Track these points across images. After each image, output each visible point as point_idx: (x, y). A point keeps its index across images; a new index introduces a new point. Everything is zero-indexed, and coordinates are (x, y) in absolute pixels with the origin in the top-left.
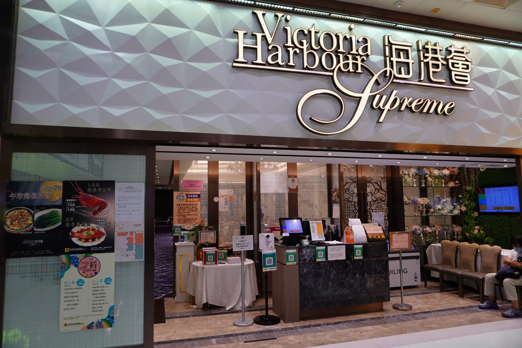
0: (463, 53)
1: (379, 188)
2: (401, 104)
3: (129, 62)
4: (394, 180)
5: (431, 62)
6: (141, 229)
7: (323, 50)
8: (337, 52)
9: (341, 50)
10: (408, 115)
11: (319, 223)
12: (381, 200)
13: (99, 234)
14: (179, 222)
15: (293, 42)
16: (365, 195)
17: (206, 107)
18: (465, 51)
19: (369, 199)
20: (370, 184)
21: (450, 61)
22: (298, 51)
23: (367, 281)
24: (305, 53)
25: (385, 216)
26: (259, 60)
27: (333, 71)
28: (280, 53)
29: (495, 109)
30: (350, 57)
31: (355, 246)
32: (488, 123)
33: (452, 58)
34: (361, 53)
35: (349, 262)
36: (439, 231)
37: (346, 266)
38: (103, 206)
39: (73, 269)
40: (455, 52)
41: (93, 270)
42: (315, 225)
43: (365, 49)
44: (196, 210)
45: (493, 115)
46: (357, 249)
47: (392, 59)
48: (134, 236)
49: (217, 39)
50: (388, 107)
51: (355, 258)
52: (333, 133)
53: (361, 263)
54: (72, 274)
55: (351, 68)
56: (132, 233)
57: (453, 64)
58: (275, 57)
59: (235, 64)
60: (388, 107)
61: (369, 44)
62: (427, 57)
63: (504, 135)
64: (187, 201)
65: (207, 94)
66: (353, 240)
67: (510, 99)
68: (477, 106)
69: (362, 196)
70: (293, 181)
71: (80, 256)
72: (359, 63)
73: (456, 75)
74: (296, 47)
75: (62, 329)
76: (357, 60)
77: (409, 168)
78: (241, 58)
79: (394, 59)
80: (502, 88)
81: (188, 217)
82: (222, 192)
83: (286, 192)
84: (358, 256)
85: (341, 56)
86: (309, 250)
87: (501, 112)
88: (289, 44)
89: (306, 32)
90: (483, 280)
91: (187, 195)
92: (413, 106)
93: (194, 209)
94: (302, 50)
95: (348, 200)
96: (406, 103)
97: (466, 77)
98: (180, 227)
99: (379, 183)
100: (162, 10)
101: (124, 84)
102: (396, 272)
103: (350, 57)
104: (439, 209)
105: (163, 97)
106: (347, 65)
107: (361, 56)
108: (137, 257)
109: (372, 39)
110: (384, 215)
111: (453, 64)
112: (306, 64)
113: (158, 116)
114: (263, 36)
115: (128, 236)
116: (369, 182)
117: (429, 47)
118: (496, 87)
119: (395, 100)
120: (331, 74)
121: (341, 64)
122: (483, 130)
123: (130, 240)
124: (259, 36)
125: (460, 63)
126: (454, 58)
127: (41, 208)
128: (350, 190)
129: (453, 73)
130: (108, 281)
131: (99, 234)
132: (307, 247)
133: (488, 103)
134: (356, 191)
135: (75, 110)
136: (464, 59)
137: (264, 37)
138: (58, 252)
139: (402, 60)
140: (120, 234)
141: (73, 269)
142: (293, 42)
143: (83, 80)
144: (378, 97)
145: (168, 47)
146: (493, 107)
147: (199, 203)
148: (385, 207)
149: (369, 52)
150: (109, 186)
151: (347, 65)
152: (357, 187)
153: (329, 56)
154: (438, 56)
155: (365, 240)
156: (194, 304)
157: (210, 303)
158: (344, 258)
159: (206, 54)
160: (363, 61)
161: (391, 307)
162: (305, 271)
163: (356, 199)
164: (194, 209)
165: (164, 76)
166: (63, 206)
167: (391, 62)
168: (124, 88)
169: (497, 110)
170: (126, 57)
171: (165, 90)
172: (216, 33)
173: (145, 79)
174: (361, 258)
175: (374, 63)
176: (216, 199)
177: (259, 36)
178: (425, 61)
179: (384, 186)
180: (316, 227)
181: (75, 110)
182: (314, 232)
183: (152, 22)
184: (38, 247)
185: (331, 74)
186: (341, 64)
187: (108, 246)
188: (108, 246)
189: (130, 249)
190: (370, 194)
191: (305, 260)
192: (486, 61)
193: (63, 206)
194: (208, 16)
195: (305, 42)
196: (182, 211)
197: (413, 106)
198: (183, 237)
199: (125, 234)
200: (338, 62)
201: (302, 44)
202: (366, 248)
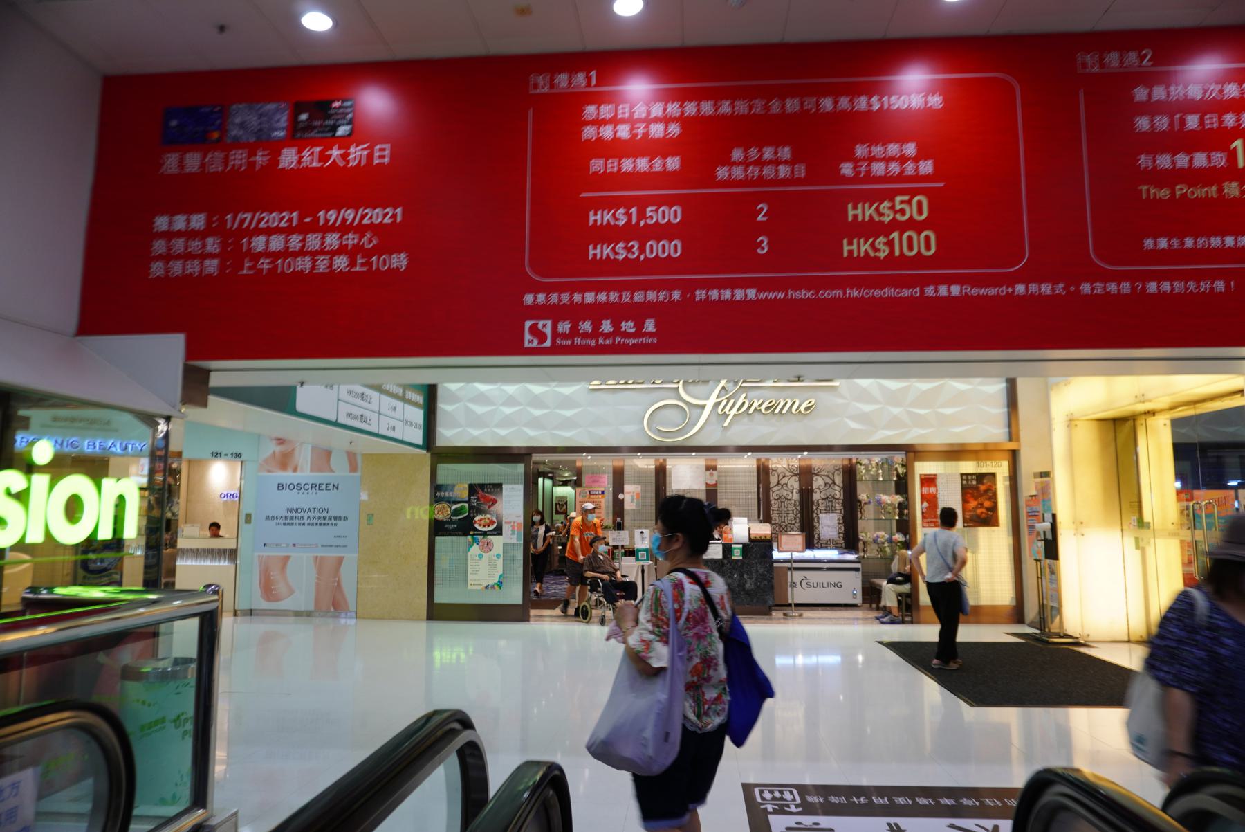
2: (749, 407)
4: (850, 474)
6: (521, 520)
13: (492, 522)
17: (568, 423)
19: (816, 496)
32: (862, 418)
37: (723, 565)
38: (495, 502)
39: (475, 546)
41: (489, 547)
50: (734, 411)
54: (475, 549)
60: (734, 411)
69: (806, 493)
70: (711, 475)
71: (480, 537)
75: (469, 587)
77: (779, 463)
82: (627, 488)
83: (704, 487)
84: (737, 555)
90: (312, 471)
92: (763, 408)
101: (508, 410)
113: (531, 433)
123: (513, 527)
127: (455, 502)
130: (498, 556)
131: (492, 522)
134: (796, 485)
135: (475, 432)
138: (466, 534)
141: (475, 546)
143: (480, 410)
148: (838, 506)
150: (498, 486)
155: (746, 540)
158: (720, 556)
163: (796, 496)
166: (469, 502)
169: (876, 401)
171: (537, 412)
176: (621, 496)
179: (839, 479)
181: (475, 432)
184: (454, 530)
187: (498, 531)
188: (498, 531)
189: (513, 533)
193: (469, 502)
197: (763, 408)
202: (746, 548)
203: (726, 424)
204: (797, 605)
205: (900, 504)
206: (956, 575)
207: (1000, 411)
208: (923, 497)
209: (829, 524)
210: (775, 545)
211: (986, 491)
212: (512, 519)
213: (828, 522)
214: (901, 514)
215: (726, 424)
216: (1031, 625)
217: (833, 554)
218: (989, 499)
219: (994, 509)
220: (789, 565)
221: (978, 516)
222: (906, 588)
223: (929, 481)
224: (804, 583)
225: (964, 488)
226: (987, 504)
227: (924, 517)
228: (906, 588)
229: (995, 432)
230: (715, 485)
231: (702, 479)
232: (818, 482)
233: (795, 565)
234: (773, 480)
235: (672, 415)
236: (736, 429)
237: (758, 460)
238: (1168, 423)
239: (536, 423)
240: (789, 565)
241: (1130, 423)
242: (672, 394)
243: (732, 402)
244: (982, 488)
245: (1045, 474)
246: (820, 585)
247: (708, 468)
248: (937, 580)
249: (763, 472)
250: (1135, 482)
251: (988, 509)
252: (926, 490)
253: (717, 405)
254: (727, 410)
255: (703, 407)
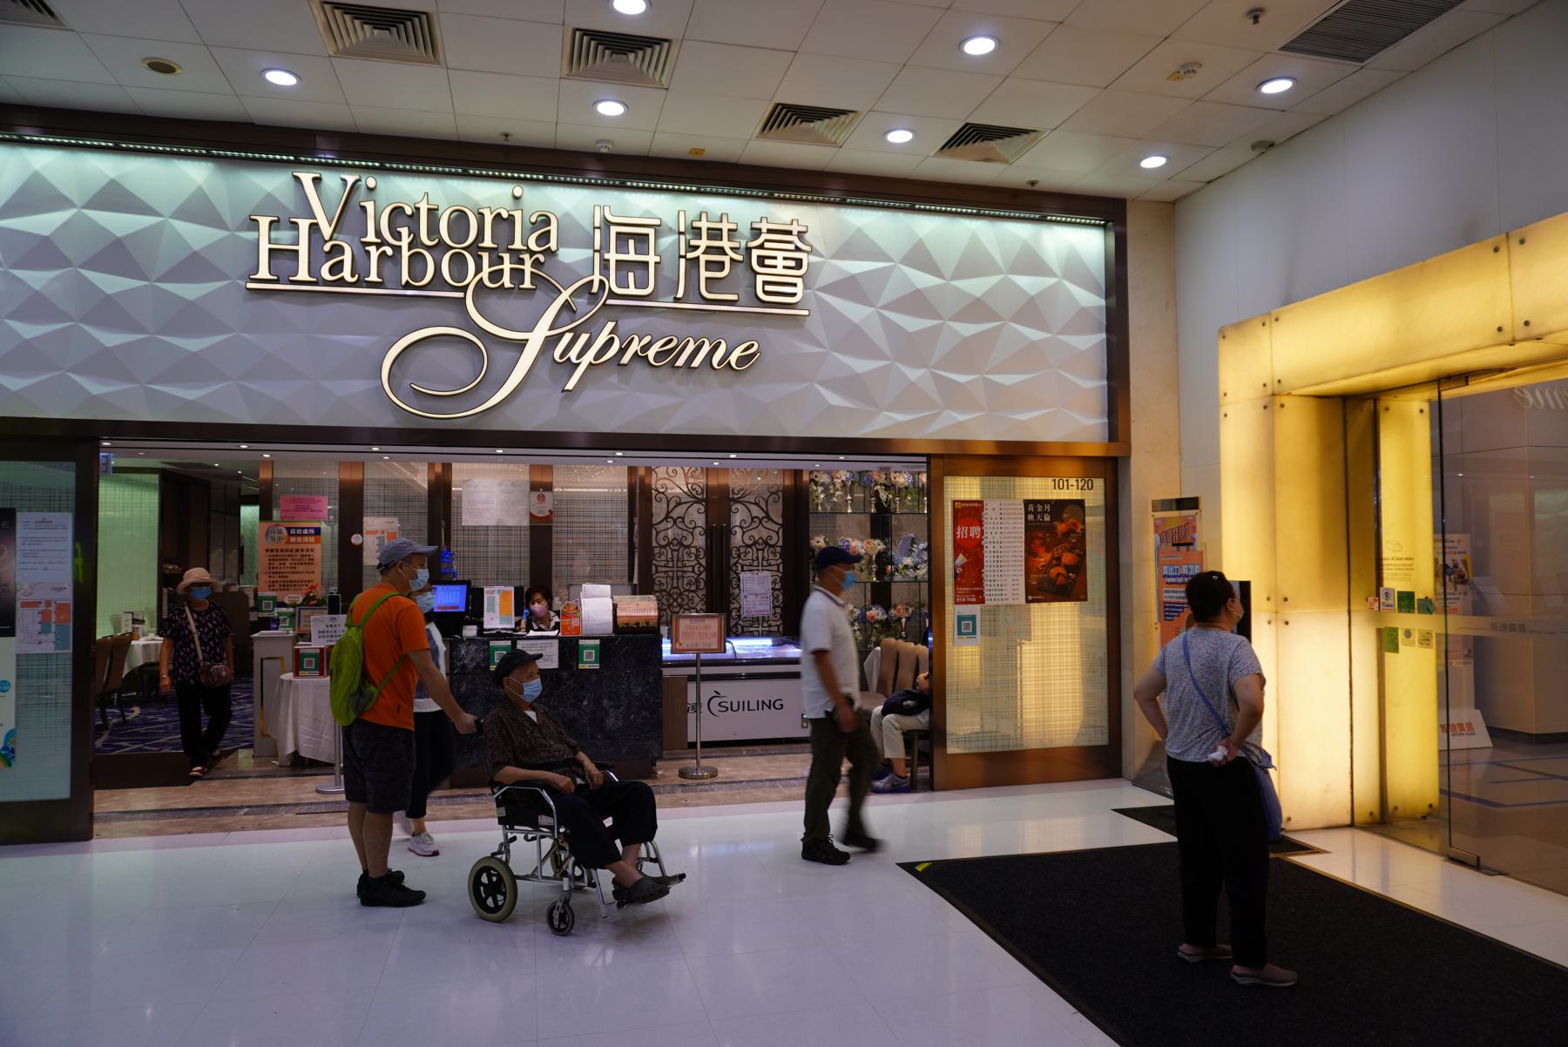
0: (789, 233)
1: (761, 514)
2: (622, 351)
3: (37, 287)
4: (796, 504)
5: (703, 259)
7: (441, 247)
8: (476, 248)
9: (488, 243)
10: (640, 371)
11: (507, 593)
12: (766, 543)
14: (271, 587)
15: (378, 234)
16: (727, 532)
17: (192, 369)
18: (795, 229)
19: (737, 539)
20: (739, 506)
21: (755, 253)
22: (389, 251)
23: (607, 714)
24: (406, 254)
25: (774, 582)
26: (303, 275)
27: (464, 289)
28: (347, 258)
29: (870, 351)
30: (506, 257)
31: (582, 642)
32: (850, 385)
33: (761, 247)
34: (534, 247)
35: (565, 674)
36: (908, 619)
40: (770, 231)
42: (497, 597)
43: (545, 237)
44: (311, 561)
45: (861, 366)
46: (586, 647)
47: (607, 256)
48: (53, 608)
49: (215, 234)
50: (589, 357)
51: (581, 666)
52: (461, 415)
53: (594, 678)
55: (506, 280)
56: (48, 603)
57: (761, 260)
58: (337, 268)
59: (250, 285)
60: (589, 357)
61: (553, 228)
62: (696, 248)
63: (890, 409)
64: (288, 542)
65: (193, 345)
66: (578, 629)
67: (910, 330)
68: (819, 344)
69: (718, 534)
70: (541, 498)
72: (528, 268)
73: (765, 283)
74: (384, 243)
76: (522, 262)
77: (675, 478)
78: (264, 273)
79: (613, 256)
80: (895, 306)
81: (292, 577)
82: (371, 522)
83: (526, 523)
85: (485, 256)
86: (473, 648)
87: (885, 358)
88: (371, 237)
89: (409, 211)
91: (288, 529)
92: (651, 353)
93: (306, 560)
94: (397, 249)
95: (681, 544)
96: (635, 347)
97: (795, 285)
98: (273, 599)
99: (763, 504)
100: (103, 182)
102: (754, 706)
103: (506, 257)
104: (906, 567)
105: (107, 353)
106: (496, 276)
107: (532, 253)
108: (58, 643)
109: (567, 215)
110: (770, 579)
111: (761, 260)
112: (405, 277)
113: (95, 388)
114: (311, 225)
115: (42, 608)
116: (737, 501)
117: (704, 225)
118: (881, 303)
119: (610, 342)
120: (461, 295)
121: (486, 270)
122: (834, 399)
123: (45, 616)
124: (304, 224)
125: (780, 255)
126: (767, 245)
128: (687, 521)
129: (760, 279)
132: (471, 640)
133: (854, 339)
134: (700, 520)
136: (792, 247)
137: (314, 228)
139: (632, 256)
140: (25, 605)
142: (378, 234)
144: (568, 337)
145: (116, 255)
146: (865, 348)
147: (317, 547)
149: (553, 245)
151: (496, 276)
152: (706, 511)
153: (458, 260)
154: (725, 243)
155: (609, 630)
156: (275, 756)
157: (303, 754)
159: (194, 266)
160: (536, 263)
161: (677, 772)
162: (463, 689)
163: (700, 541)
164: (306, 560)
165: (109, 312)
167: (605, 264)
168: (27, 336)
170: (37, 279)
171: (111, 339)
172: (218, 223)
173: (70, 319)
174: (597, 666)
175: (567, 267)
176: (356, 539)
177: (304, 224)
178: (690, 255)
179: (776, 512)
180: (497, 600)
182: (492, 610)
183: (86, 207)
185: (461, 295)
186: (485, 274)
189: (45, 629)
190: (738, 530)
191: (464, 666)
192: (854, 247)
194: (200, 189)
195: (404, 231)
196: (277, 564)
197: (651, 353)
198: (277, 621)
199: (35, 604)
200: (479, 269)
201: (398, 236)
202: (607, 645)
203: (570, 386)
204: (705, 745)
205: (879, 555)
206: (1241, 743)
207: (1094, 385)
208: (959, 547)
209: (756, 590)
210: (664, 630)
211: (1067, 534)
212: (41, 595)
213: (756, 588)
214: (881, 573)
215: (570, 386)
216: (1138, 782)
217: (758, 646)
218: (1071, 550)
219: (1079, 567)
220: (692, 671)
221: (1052, 582)
222: (921, 720)
223: (970, 513)
224: (715, 702)
225: (1029, 528)
226: (1068, 558)
227: (957, 584)
228: (921, 720)
229: (1075, 420)
230: (548, 518)
231: (523, 507)
232: (738, 516)
233: (705, 670)
234: (659, 510)
235: (453, 361)
236: (590, 396)
237: (632, 471)
238: (1426, 407)
239: (104, 363)
240: (692, 671)
241: (1369, 405)
242: (451, 315)
243: (584, 338)
244: (1061, 528)
245: (1192, 503)
246: (745, 706)
247: (534, 487)
248: (1191, 757)
249: (640, 496)
250: (1373, 512)
251: (1068, 568)
252: (962, 532)
253: (551, 342)
254: (573, 355)
255: (522, 344)
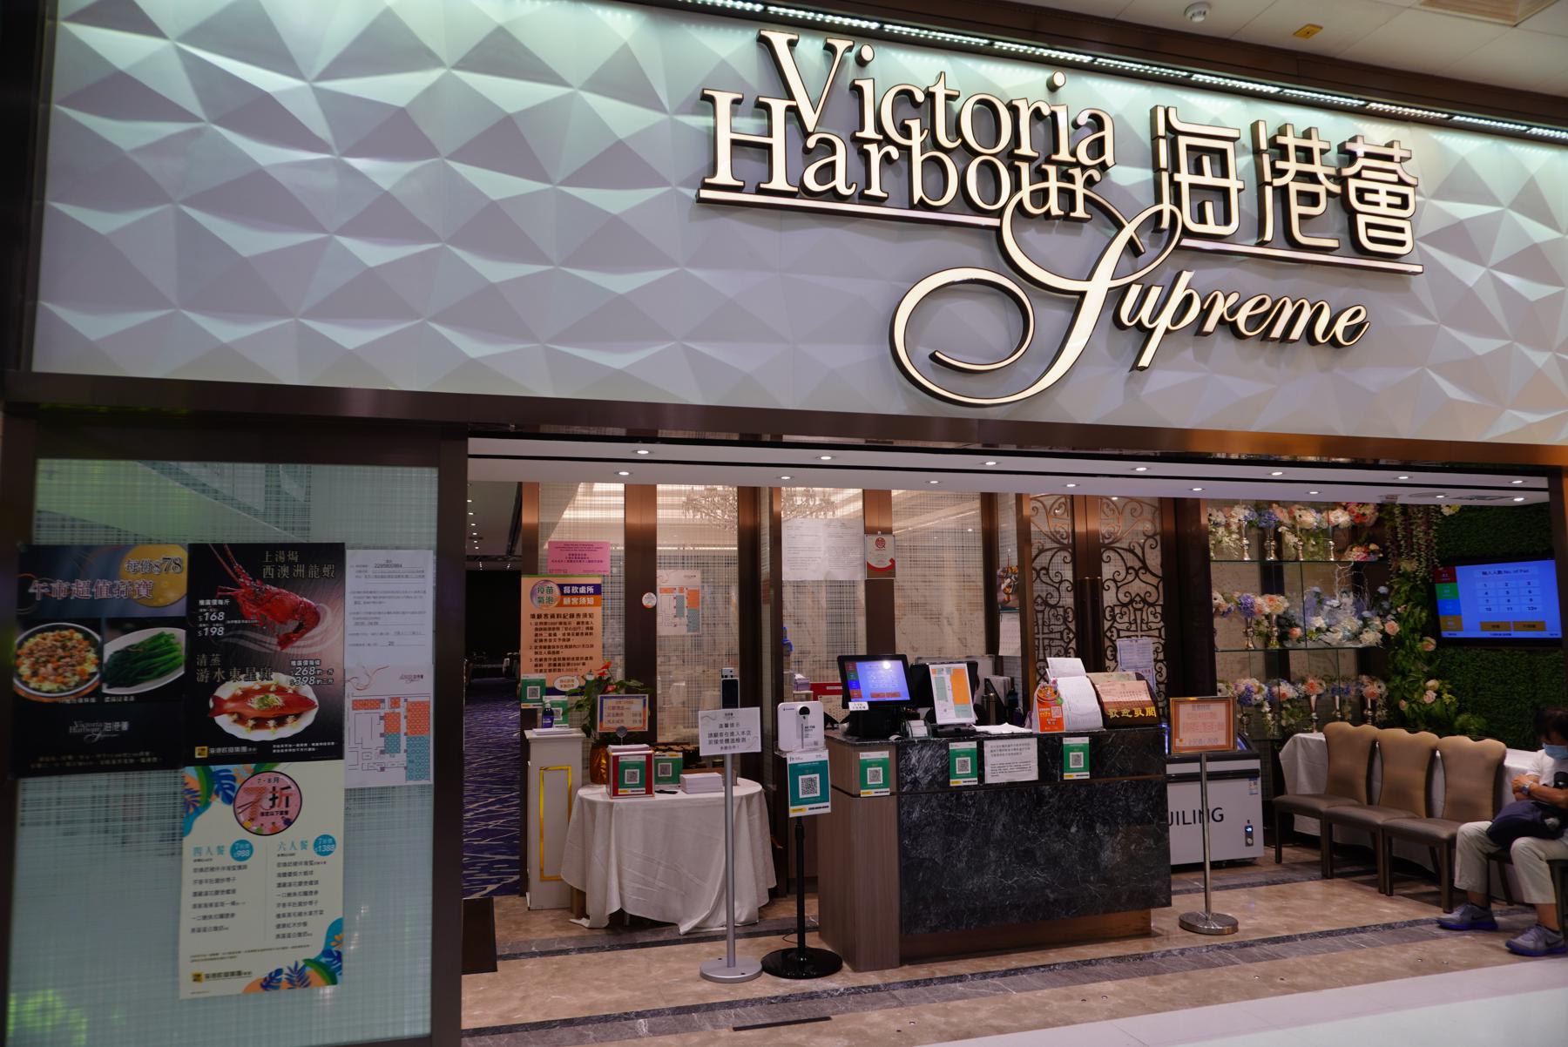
0: (1390, 158)
1: (1137, 564)
2: (1205, 314)
3: (386, 185)
4: (1182, 540)
5: (1294, 187)
6: (425, 690)
7: (969, 152)
8: (1011, 157)
9: (1025, 150)
10: (1224, 345)
11: (957, 671)
12: (1144, 601)
13: (297, 705)
14: (538, 667)
15: (879, 127)
16: (1097, 587)
17: (618, 321)
18: (1396, 152)
19: (1109, 598)
20: (1112, 554)
21: (1353, 184)
22: (895, 153)
23: (1101, 846)
24: (917, 159)
25: (1156, 651)
26: (779, 182)
27: (999, 214)
28: (840, 158)
29: (1486, 327)
30: (1052, 170)
31: (1067, 741)
32: (1467, 370)
33: (1358, 176)
34: (1084, 158)
35: (1047, 789)
36: (1319, 696)
37: (1040, 800)
38: (309, 619)
39: (219, 810)
40: (1368, 155)
41: (280, 811)
42: (947, 677)
43: (1098, 147)
44: (590, 631)
45: (1481, 345)
46: (1073, 749)
47: (1177, 177)
48: (402, 710)
49: (650, 117)
50: (1164, 321)
51: (1067, 776)
52: (1001, 402)
53: (1083, 792)
54: (217, 823)
55: (1053, 205)
56: (395, 702)
57: (1361, 193)
58: (827, 172)
59: (705, 194)
60: (1164, 321)
61: (1108, 133)
62: (1283, 173)
63: (1514, 407)
64: (561, 605)
65: (621, 283)
66: (1059, 722)
67: (1532, 298)
68: (1432, 318)
69: (1088, 589)
70: (880, 544)
71: (240, 770)
72: (1079, 188)
73: (1369, 226)
74: (888, 140)
75: (188, 989)
76: (1071, 179)
78: (724, 176)
79: (1185, 178)
80: (1507, 266)
81: (566, 653)
82: (666, 577)
83: (860, 577)
84: (1076, 769)
85: (1025, 168)
86: (927, 753)
87: (1505, 337)
88: (869, 132)
89: (920, 97)
90: (1452, 841)
91: (561, 587)
92: (1241, 318)
93: (583, 629)
94: (906, 151)
95: (1045, 603)
96: (1220, 309)
97: (1401, 230)
98: (541, 683)
99: (1138, 551)
100: (486, 30)
101: (372, 254)
102: (1189, 818)
103: (1052, 170)
104: (1318, 630)
105: (491, 292)
106: (1041, 196)
107: (1084, 168)
108: (410, 772)
109: (1119, 117)
110: (1152, 648)
111: (1361, 193)
112: (918, 193)
113: (474, 348)
114: (789, 109)
115: (386, 709)
116: (1109, 547)
117: (1290, 141)
118: (1491, 263)
119: (1188, 300)
120: (995, 222)
121: (1025, 194)
122: (1452, 391)
123: (390, 721)
124: (779, 107)
125: (1383, 188)
126: (1365, 174)
127: (122, 624)
128: (1052, 573)
129: (1362, 220)
130: (323, 844)
131: (297, 705)
132: (924, 742)
133: (1466, 309)
134: (1068, 574)
135: (226, 332)
136: (1394, 178)
137: (793, 112)
138: (173, 759)
139: (1208, 179)
140: (359, 705)
141: (219, 810)
142: (879, 127)
143: (248, 241)
144: (1135, 291)
145: (504, 142)
146: (1480, 323)
147: (598, 611)
148: (1156, 623)
149: (1108, 157)
150: (327, 559)
151: (1041, 196)
152: (1074, 561)
153: (989, 169)
154: (1317, 168)
155: (1096, 722)
156: (582, 913)
157: (630, 911)
158: (1033, 775)
159: (618, 163)
160: (1090, 182)
161: (1176, 923)
162: (915, 815)
163: (1068, 600)
164: (583, 629)
165: (493, 229)
166: (189, 621)
167: (1176, 187)
168: (371, 264)
169: (1492, 330)
170: (379, 171)
171: (497, 271)
172: (650, 100)
173: (436, 239)
174: (1086, 775)
175: (1123, 191)
176: (648, 600)
177: (779, 107)
178: (1278, 182)
179: (1154, 559)
180: (948, 683)
181: (226, 332)
182: (944, 697)
183: (457, 67)
184: (114, 744)
185: (995, 222)
186: (1025, 194)
187: (326, 740)
188: (326, 740)
189: (390, 748)
190: (1112, 584)
191: (915, 782)
192: (1459, 184)
193: (189, 621)
194: (625, 48)
195: (915, 125)
196: (545, 635)
197: (1241, 318)
198: (549, 714)
199: (375, 704)
200: (1016, 186)
201: (906, 131)
202: (1098, 745)
